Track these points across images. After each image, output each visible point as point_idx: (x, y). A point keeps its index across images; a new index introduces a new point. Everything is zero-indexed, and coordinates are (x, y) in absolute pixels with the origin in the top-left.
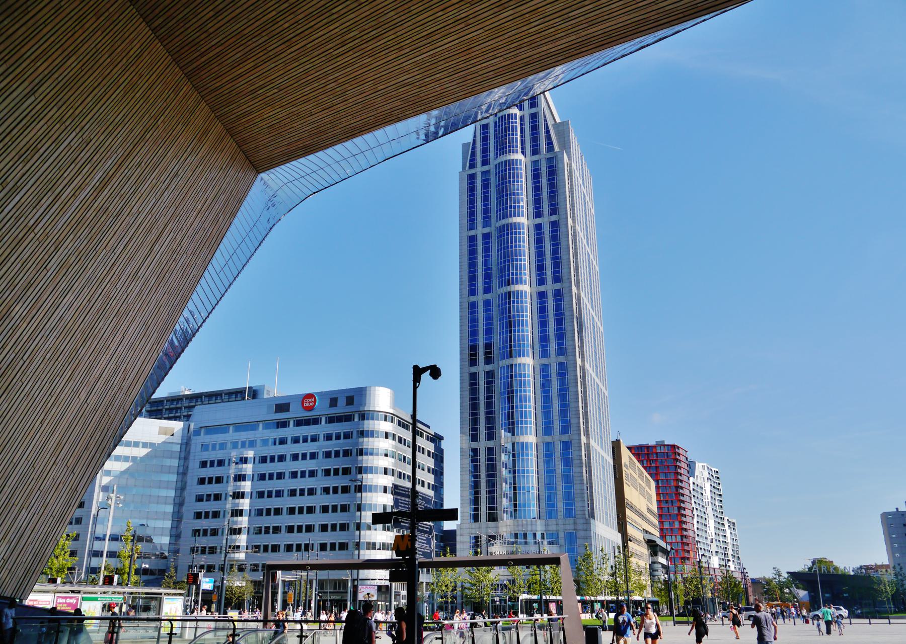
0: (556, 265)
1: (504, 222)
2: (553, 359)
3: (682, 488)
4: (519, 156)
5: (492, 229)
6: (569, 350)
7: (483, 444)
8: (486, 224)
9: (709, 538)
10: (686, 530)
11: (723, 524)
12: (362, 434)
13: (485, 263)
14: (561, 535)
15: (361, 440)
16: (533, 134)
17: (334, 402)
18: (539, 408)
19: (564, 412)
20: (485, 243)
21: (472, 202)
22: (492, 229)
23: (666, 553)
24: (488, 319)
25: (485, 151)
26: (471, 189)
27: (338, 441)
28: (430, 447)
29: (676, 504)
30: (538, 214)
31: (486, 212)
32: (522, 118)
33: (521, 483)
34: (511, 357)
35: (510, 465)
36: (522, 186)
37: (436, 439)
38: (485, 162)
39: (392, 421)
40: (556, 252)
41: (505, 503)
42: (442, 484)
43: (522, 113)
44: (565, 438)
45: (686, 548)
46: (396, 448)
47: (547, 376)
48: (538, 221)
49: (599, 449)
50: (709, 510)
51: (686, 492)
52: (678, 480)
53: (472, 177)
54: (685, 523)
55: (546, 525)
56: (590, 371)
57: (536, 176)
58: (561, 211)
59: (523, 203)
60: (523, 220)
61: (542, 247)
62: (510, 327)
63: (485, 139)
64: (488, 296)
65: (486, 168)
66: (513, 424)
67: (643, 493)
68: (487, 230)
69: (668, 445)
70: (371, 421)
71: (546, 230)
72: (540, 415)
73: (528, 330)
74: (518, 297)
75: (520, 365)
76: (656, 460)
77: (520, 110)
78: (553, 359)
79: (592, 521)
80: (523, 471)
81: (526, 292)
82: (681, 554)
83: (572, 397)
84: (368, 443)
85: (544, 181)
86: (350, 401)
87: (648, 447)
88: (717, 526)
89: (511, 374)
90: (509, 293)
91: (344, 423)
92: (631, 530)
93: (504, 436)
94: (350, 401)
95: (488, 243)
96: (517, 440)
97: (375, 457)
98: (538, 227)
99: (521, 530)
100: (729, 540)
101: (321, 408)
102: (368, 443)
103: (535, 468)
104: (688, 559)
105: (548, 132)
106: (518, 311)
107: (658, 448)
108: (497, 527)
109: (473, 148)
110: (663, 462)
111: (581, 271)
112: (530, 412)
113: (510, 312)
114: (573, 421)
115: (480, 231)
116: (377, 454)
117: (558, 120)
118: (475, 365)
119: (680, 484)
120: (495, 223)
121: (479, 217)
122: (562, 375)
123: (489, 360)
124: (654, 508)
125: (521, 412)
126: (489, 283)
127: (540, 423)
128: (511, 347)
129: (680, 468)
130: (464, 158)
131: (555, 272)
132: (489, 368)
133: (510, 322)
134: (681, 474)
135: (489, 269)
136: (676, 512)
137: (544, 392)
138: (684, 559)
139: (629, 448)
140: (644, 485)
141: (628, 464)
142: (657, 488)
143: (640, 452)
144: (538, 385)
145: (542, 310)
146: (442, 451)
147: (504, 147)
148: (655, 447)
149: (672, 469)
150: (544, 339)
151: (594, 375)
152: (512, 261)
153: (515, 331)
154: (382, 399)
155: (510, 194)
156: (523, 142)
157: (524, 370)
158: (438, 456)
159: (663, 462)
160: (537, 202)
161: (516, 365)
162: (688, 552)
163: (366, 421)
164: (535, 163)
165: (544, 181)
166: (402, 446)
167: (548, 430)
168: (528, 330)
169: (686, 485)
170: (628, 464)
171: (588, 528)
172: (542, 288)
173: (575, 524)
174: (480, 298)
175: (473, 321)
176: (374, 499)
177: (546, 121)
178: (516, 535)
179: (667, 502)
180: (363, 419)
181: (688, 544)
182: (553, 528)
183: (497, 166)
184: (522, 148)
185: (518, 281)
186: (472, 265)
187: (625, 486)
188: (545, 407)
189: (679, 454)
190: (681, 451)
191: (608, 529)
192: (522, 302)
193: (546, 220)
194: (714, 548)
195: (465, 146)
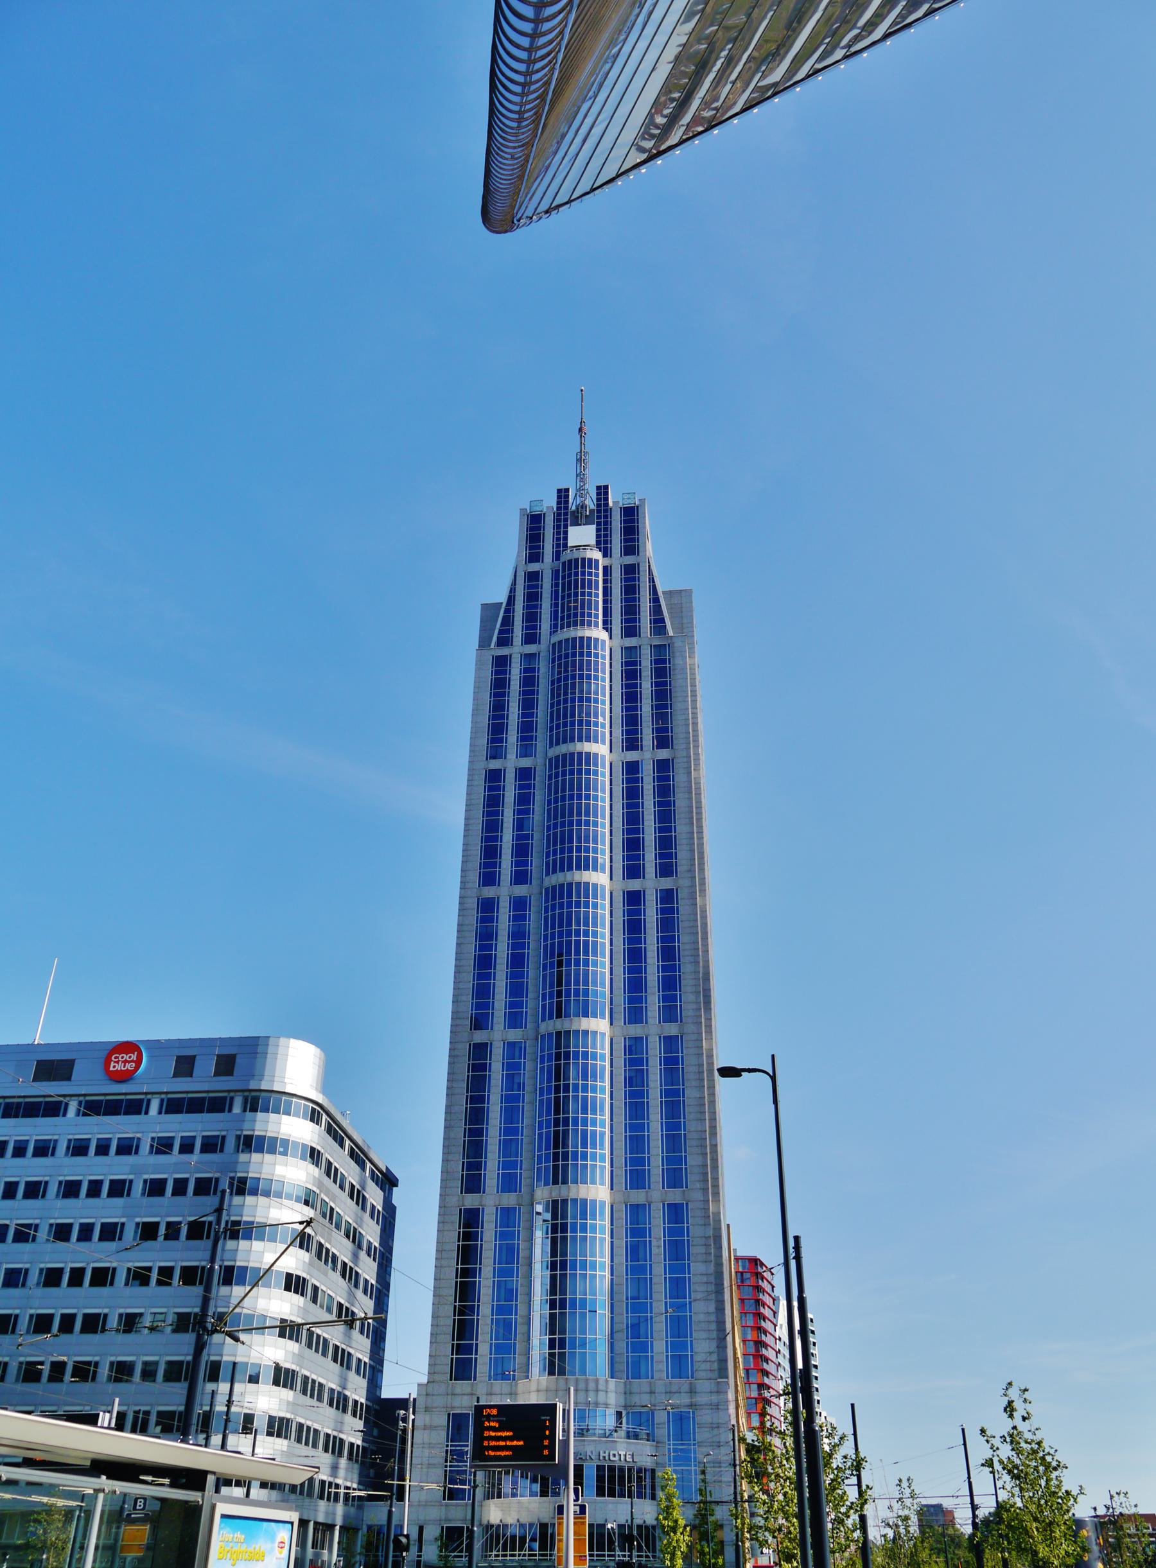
0: (666, 843)
1: (563, 749)
2: (654, 1028)
4: (603, 635)
5: (535, 763)
8: (526, 749)
12: (250, 1143)
13: (519, 825)
14: (661, 1417)
17: (185, 1066)
18: (621, 1129)
21: (498, 707)
22: (535, 763)
24: (518, 935)
25: (532, 618)
27: (185, 1157)
28: (374, 1195)
31: (527, 728)
38: (531, 637)
40: (665, 816)
43: (607, 562)
46: (320, 1184)
47: (640, 1062)
48: (632, 756)
53: (501, 663)
55: (627, 1393)
57: (631, 673)
59: (604, 720)
60: (602, 749)
61: (637, 805)
63: (533, 597)
64: (521, 890)
65: (531, 649)
66: (566, 1158)
68: (526, 762)
69: (743, 1258)
70: (273, 1116)
72: (621, 1145)
73: (603, 967)
75: (586, 1032)
77: (605, 555)
78: (654, 1028)
85: (646, 686)
91: (206, 1116)
94: (226, 1065)
98: (632, 768)
101: (154, 1077)
109: (507, 611)
115: (511, 762)
116: (279, 1195)
121: (512, 737)
122: (672, 1062)
126: (525, 863)
127: (620, 1161)
135: (527, 837)
137: (633, 1094)
145: (634, 927)
147: (570, 611)
150: (635, 985)
154: (298, 1067)
155: (581, 700)
156: (607, 612)
161: (577, 1032)
163: (260, 1115)
165: (646, 686)
166: (328, 1182)
167: (637, 1177)
168: (603, 967)
172: (635, 885)
173: (692, 1391)
174: (505, 892)
175: (486, 937)
177: (652, 580)
180: (254, 1109)
183: (555, 647)
184: (605, 623)
186: (492, 827)
188: (633, 1127)
193: (647, 756)
195: (489, 610)
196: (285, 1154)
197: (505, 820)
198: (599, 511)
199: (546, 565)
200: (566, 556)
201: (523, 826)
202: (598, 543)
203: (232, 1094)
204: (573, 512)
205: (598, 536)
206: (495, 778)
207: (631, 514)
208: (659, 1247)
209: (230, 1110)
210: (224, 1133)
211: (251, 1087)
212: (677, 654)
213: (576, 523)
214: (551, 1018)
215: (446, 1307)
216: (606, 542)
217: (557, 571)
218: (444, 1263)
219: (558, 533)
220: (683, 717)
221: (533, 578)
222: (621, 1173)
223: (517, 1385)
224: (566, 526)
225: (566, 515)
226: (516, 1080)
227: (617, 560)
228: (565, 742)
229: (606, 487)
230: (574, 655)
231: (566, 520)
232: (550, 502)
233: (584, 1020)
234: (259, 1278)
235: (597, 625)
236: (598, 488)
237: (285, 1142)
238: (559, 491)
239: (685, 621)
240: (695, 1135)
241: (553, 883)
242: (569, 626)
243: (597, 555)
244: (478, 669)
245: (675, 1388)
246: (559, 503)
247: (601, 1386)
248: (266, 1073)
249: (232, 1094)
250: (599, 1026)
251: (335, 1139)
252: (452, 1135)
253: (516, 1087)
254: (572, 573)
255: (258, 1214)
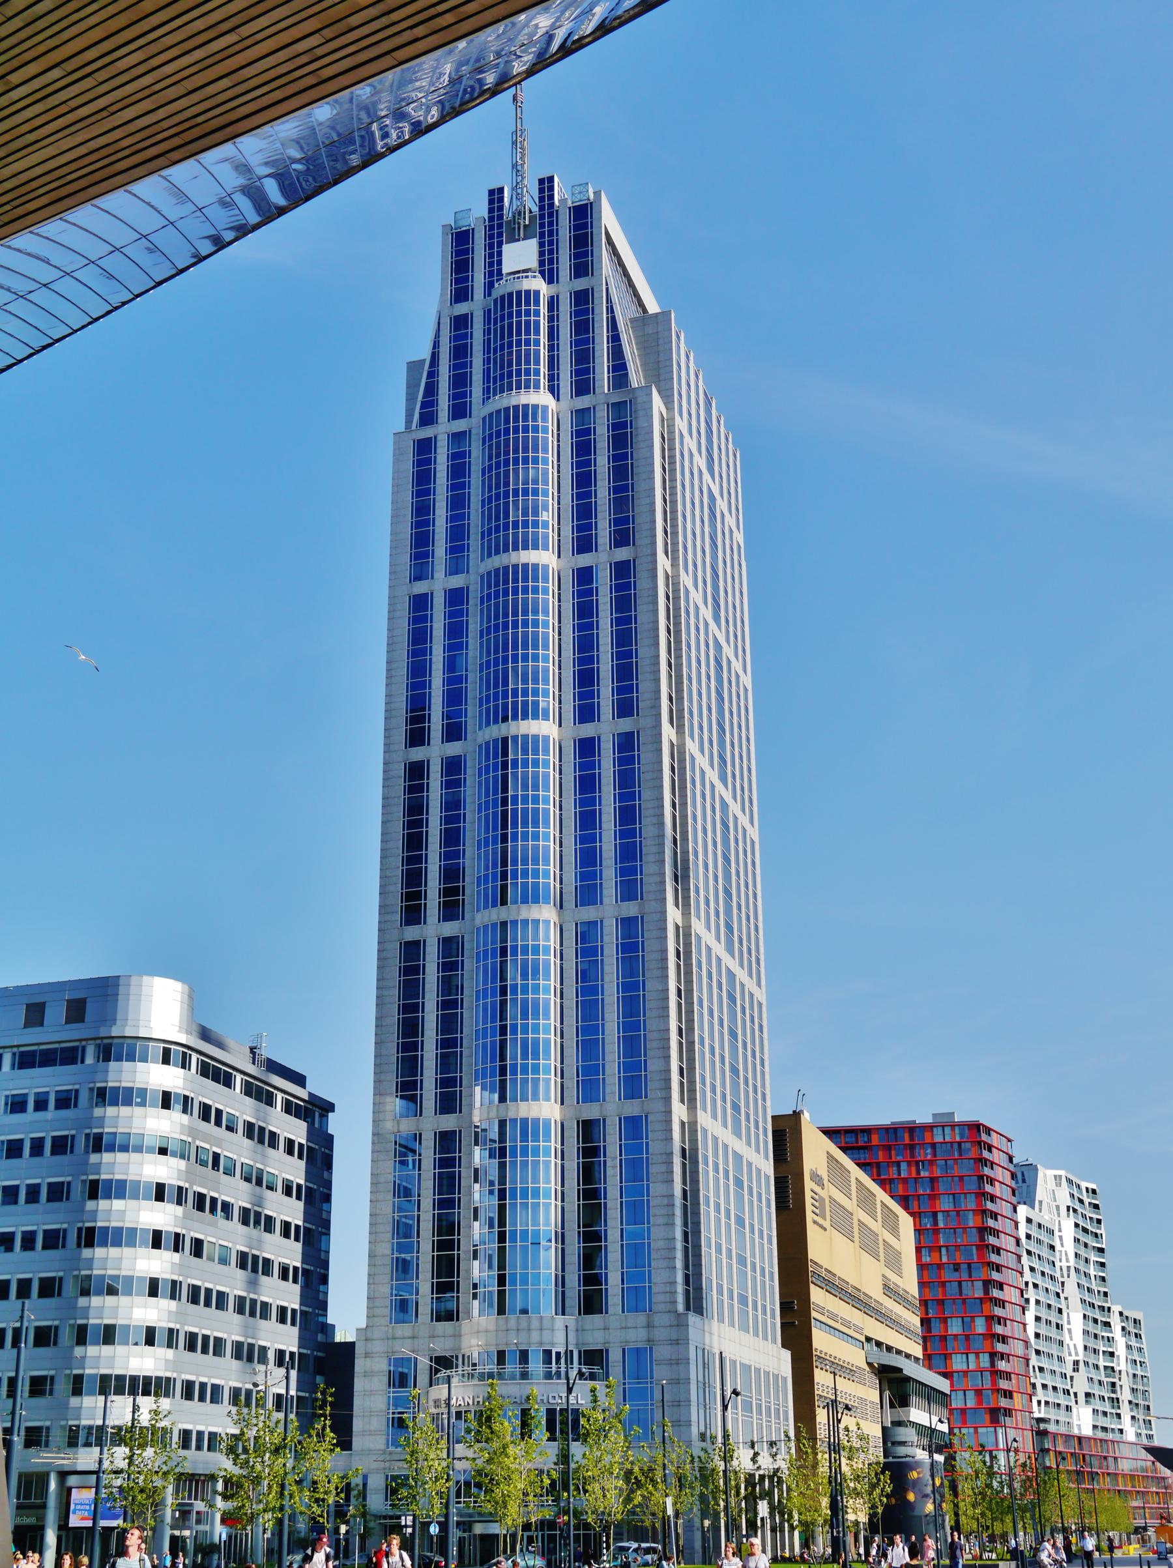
0: (625, 672)
1: (497, 561)
3: (996, 1233)
4: (541, 397)
5: (470, 581)
6: (649, 884)
7: (432, 1122)
9: (1070, 1360)
10: (1004, 1339)
11: (1107, 1324)
13: (451, 665)
14: (615, 1356)
15: (98, 1112)
16: (578, 343)
19: (632, 1042)
20: (451, 615)
21: (422, 510)
22: (470, 581)
23: (932, 1396)
24: (453, 806)
25: (460, 381)
26: (423, 478)
27: (40, 1115)
28: (296, 1130)
29: (980, 1273)
30: (584, 544)
31: (457, 535)
32: (553, 303)
33: (518, 1221)
34: (504, 902)
35: (494, 1175)
36: (546, 472)
37: (315, 1111)
38: (459, 410)
39: (185, 1065)
41: (477, 1271)
42: (326, 1224)
44: (633, 1108)
45: (1003, 1384)
48: (585, 560)
49: (726, 1136)
50: (1071, 1289)
51: (1007, 1242)
52: (984, 1212)
53: (424, 448)
54: (1001, 1320)
56: (708, 938)
57: (583, 447)
58: (641, 538)
59: (548, 516)
62: (504, 826)
63: (461, 352)
64: (454, 749)
65: (460, 425)
67: (869, 1244)
68: (457, 582)
69: (961, 1125)
70: (140, 1065)
71: (604, 583)
74: (525, 751)
75: (525, 922)
76: (932, 1163)
77: (550, 282)
79: (693, 1318)
80: (525, 1191)
81: (546, 739)
82: (990, 1401)
83: (651, 1004)
84: (120, 1119)
85: (602, 463)
86: (76, 1011)
87: (912, 1129)
88: (1091, 1327)
89: (503, 946)
90: (505, 740)
91: (58, 1069)
92: (821, 1341)
93: (480, 1104)
94: (76, 1011)
95: (460, 613)
96: (511, 1114)
97: (134, 1156)
98: (584, 576)
99: (513, 1342)
100: (1122, 1365)
102: (120, 1119)
103: (553, 1185)
104: (1008, 1412)
105: (615, 338)
106: (525, 787)
107: (938, 1132)
108: (458, 1336)
110: (938, 1173)
111: (691, 689)
112: (547, 1042)
113: (505, 789)
114: (654, 1065)
115: (440, 583)
116: (139, 1149)
117: (653, 307)
118: (417, 921)
119: (991, 1223)
120: (479, 565)
122: (630, 949)
123: (451, 909)
124: (909, 1282)
125: (525, 1042)
128: (504, 876)
129: (992, 1181)
130: (410, 398)
131: (620, 690)
132: (450, 929)
133: (505, 814)
134: (993, 1198)
135: (459, 680)
136: (979, 1293)
138: (996, 1416)
139: (829, 1133)
140: (875, 1226)
141: (823, 1172)
142: (919, 1231)
143: (850, 1139)
144: (570, 974)
145: (587, 784)
146: (330, 1139)
147: (506, 373)
148: (929, 1128)
149: (971, 1185)
151: (719, 949)
152: (515, 659)
153: (515, 839)
154: (160, 1008)
156: (553, 363)
157: (536, 937)
158: (319, 1155)
159: (938, 1173)
160: (584, 512)
162: (1008, 1394)
164: (582, 415)
165: (602, 463)
166: (210, 1128)
167: (589, 1084)
169: (1008, 1226)
170: (823, 1172)
171: (680, 1341)
173: (649, 1326)
174: (436, 752)
175: (415, 810)
176: (125, 1264)
177: (611, 310)
178: (501, 1355)
179: (957, 1267)
180: (107, 1059)
181: (1007, 1376)
182: (595, 1341)
184: (551, 378)
185: (530, 711)
187: (812, 1231)
189: (990, 1148)
190: (994, 1140)
191: (748, 1339)
192: (536, 763)
193: (603, 559)
194: (1081, 1385)
195: (414, 367)
196: (143, 1104)
197: (434, 660)
198: (542, 217)
199: (476, 306)
200: (500, 289)
201: (450, 670)
202: (541, 263)
203: (84, 1043)
204: (509, 222)
205: (541, 254)
206: (420, 603)
207: (583, 214)
208: (614, 1167)
209: (83, 1062)
210: (77, 1087)
211: (102, 1035)
212: (641, 413)
213: (513, 239)
214: (486, 907)
215: (384, 1245)
216: (551, 261)
217: (489, 310)
218: (380, 1196)
219: (491, 256)
220: (648, 501)
221: (461, 323)
222: (571, 1085)
223: (460, 1326)
224: (500, 244)
225: (500, 226)
226: (454, 983)
227: (567, 285)
228: (497, 552)
229: (551, 179)
230: (507, 432)
231: (500, 235)
232: (480, 210)
233: (524, 907)
234: (119, 1237)
235: (537, 386)
236: (541, 181)
237: (143, 1092)
238: (491, 192)
239: (662, 357)
240: (656, 1035)
241: (487, 738)
242: (502, 391)
243: (538, 284)
244: (397, 461)
245: (631, 1323)
246: (491, 210)
247: (546, 1324)
248: (118, 1017)
249: (84, 1043)
250: (547, 913)
251: (216, 1079)
252: (384, 1052)
253: (454, 991)
254: (509, 310)
255: (131, 1171)
